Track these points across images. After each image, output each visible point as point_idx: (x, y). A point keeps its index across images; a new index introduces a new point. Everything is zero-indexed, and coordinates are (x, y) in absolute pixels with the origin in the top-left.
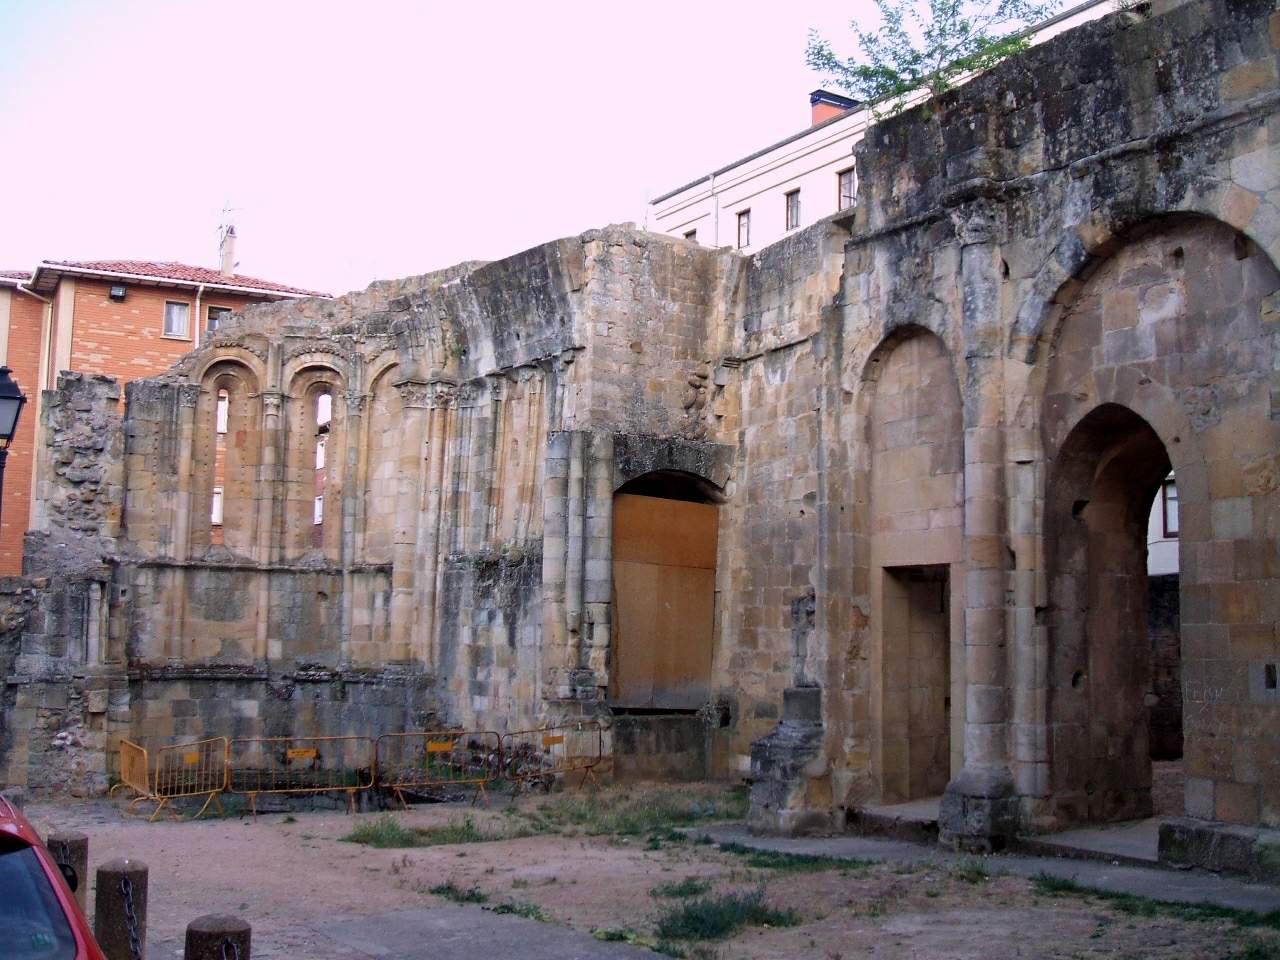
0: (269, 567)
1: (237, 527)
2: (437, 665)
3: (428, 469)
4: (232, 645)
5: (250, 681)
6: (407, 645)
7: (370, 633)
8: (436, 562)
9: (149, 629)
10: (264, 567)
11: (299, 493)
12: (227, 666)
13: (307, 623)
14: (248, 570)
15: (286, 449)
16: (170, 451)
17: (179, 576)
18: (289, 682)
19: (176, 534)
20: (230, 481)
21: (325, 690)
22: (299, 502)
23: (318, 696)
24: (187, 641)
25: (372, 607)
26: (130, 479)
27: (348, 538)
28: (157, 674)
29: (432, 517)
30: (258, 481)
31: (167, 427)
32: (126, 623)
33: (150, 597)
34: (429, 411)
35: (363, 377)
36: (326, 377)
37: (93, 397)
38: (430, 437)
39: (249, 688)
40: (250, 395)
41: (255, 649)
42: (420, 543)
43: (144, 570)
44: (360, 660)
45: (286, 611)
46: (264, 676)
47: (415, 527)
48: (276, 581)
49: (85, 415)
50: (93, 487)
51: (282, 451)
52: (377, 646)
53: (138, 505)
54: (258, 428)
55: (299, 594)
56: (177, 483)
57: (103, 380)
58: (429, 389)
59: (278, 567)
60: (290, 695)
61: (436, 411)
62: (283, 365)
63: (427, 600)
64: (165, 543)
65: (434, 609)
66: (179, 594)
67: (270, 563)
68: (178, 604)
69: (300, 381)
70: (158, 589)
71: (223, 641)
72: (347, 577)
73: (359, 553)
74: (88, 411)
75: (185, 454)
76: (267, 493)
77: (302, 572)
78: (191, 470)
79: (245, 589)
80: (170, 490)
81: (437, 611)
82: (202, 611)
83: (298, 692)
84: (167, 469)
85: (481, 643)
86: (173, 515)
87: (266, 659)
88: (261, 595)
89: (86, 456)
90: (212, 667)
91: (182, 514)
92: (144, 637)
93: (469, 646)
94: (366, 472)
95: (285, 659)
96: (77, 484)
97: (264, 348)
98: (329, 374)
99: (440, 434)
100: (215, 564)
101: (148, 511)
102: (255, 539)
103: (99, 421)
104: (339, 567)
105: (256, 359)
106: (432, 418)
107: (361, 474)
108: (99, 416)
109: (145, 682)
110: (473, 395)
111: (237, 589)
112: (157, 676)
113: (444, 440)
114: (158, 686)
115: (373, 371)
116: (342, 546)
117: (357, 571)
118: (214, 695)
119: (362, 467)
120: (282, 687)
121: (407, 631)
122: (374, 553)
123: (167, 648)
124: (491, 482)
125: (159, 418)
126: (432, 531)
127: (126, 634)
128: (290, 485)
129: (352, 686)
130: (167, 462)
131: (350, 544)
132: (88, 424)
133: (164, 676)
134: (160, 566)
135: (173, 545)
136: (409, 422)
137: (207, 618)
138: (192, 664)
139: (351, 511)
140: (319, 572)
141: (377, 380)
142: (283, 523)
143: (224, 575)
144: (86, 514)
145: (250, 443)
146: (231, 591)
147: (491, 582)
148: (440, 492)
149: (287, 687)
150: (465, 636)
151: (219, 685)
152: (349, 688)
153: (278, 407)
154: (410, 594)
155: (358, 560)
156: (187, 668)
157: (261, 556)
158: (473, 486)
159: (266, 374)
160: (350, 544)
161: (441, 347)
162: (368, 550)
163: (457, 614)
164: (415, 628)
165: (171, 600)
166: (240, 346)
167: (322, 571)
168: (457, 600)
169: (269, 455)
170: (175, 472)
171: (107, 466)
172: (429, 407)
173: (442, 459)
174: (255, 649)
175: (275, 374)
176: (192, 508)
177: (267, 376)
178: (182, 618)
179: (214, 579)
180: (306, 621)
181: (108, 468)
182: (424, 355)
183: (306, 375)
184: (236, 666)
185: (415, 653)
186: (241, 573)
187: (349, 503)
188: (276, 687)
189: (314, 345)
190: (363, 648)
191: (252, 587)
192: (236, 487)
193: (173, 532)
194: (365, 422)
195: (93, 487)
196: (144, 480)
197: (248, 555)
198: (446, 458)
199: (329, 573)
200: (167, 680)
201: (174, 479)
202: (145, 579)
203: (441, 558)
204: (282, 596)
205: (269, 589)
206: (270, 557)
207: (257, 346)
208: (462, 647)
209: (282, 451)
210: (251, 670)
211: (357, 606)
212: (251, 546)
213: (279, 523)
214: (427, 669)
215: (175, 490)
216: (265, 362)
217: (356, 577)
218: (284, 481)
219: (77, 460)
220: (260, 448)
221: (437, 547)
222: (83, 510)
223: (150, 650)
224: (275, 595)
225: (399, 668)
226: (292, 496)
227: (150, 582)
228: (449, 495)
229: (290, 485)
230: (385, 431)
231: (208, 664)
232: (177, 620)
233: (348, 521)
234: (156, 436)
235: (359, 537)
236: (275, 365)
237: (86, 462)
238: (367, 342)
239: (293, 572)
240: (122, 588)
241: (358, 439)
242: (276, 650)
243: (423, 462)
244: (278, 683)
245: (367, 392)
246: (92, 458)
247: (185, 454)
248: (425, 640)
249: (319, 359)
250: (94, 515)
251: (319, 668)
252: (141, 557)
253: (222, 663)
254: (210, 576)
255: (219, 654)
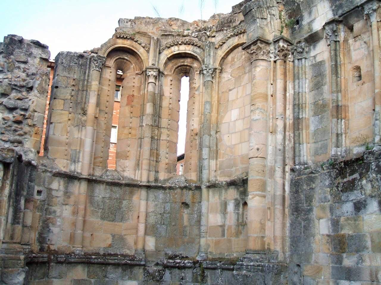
0: (148, 184)
1: (126, 157)
2: (288, 254)
3: (274, 103)
4: (119, 239)
5: (132, 266)
6: (263, 237)
7: (223, 231)
8: (284, 171)
9: (58, 223)
10: (144, 184)
11: (168, 136)
12: (116, 255)
13: (167, 225)
14: (133, 186)
15: (160, 106)
16: (82, 98)
17: (84, 186)
18: (160, 268)
19: (83, 156)
20: (122, 127)
21: (188, 274)
22: (168, 141)
23: (182, 279)
24: (88, 234)
25: (224, 211)
26: (53, 115)
27: (206, 163)
28: (62, 258)
29: (280, 137)
30: (142, 126)
31: (81, 83)
32: (41, 216)
33: (61, 200)
34: (272, 63)
35: (215, 57)
36: (187, 62)
37: (30, 55)
38: (275, 80)
39: (131, 272)
40: (137, 72)
41: (136, 243)
42: (270, 157)
43: (57, 179)
44: (215, 252)
45: (159, 216)
46: (143, 263)
47: (266, 145)
48: (152, 194)
49: (22, 66)
50: (23, 113)
51: (158, 107)
52: (230, 241)
53: (59, 134)
54: (142, 93)
55: (169, 204)
56: (86, 121)
57: (38, 44)
58: (272, 48)
59: (153, 184)
60: (161, 278)
61: (278, 62)
62: (160, 53)
63: (279, 201)
64: (75, 162)
65: (284, 210)
66: (82, 199)
67: (148, 182)
68: (82, 207)
69: (170, 65)
70: (67, 194)
71: (113, 236)
72: (204, 190)
73: (213, 173)
74: (25, 63)
75: (93, 100)
76: (147, 133)
77: (170, 188)
78: (96, 114)
79: (130, 200)
80: (81, 125)
81: (287, 210)
82: (99, 214)
83: (167, 275)
84: (80, 111)
85: (347, 231)
86: (82, 143)
87: (144, 250)
88: (142, 204)
89: (20, 92)
90: (104, 255)
91: (88, 142)
92: (55, 230)
93: (328, 236)
94: (217, 118)
95: (158, 251)
96: (11, 110)
97: (148, 42)
98: (189, 60)
99: (282, 77)
100: (110, 180)
101: (64, 138)
102: (138, 165)
103: (33, 70)
104: (198, 184)
105: (142, 49)
106: (275, 68)
107: (214, 119)
108: (33, 68)
109: (52, 264)
110: (307, 49)
111: (124, 200)
112: (62, 260)
113: (285, 82)
114: (64, 268)
115: (221, 53)
116: (200, 169)
117: (213, 186)
118: (105, 276)
119: (214, 114)
120: (155, 271)
121: (263, 227)
122: (223, 174)
123: (72, 238)
124: (337, 101)
125: (75, 77)
126: (280, 147)
127: (38, 225)
128: (162, 130)
129: (210, 271)
130: (79, 107)
131: (207, 167)
132: (24, 71)
133: (68, 260)
134: (70, 178)
135: (80, 163)
136: (258, 69)
137: (103, 218)
138: (90, 252)
139: (207, 144)
140: (182, 188)
141: (224, 58)
142: (158, 155)
143: (115, 189)
144: (15, 131)
145: (136, 102)
146: (120, 200)
147: (356, 175)
148: (284, 118)
149: (159, 271)
150: (322, 227)
151: (109, 268)
152: (207, 273)
153: (156, 77)
154: (264, 197)
155: (212, 179)
156: (87, 255)
157: (142, 176)
158: (312, 113)
159: (148, 59)
160: (207, 167)
161: (279, 20)
162: (219, 172)
163: (310, 210)
164: (269, 224)
165: (76, 204)
166: (133, 39)
167: (185, 187)
168: (309, 199)
169: (149, 109)
170: (85, 113)
171: (34, 99)
172: (272, 60)
173: (285, 95)
174: (136, 243)
175: (155, 56)
176: (95, 141)
177: (149, 59)
178: (85, 216)
179: (108, 191)
180: (173, 224)
181: (36, 100)
182: (267, 25)
183: (174, 61)
184: (122, 255)
185: (269, 245)
186: (127, 188)
187: (206, 138)
188: (151, 271)
189: (180, 40)
190: (217, 243)
191: (135, 198)
192: (126, 131)
193: (81, 155)
194: (215, 86)
195: (23, 113)
196: (63, 116)
197: (132, 177)
198: (288, 95)
199: (190, 189)
200: (70, 263)
201: (84, 118)
202: (57, 185)
203: (287, 169)
204: (156, 205)
205: (147, 200)
206: (148, 177)
207: (143, 40)
208: (318, 237)
209: (158, 107)
210: (133, 258)
211: (214, 213)
212: (135, 170)
213: (155, 154)
214: (281, 258)
215: (84, 126)
216: (148, 51)
217: (211, 191)
218: (158, 127)
219: (14, 94)
220: (143, 106)
221: (284, 161)
222: (13, 128)
223: (58, 239)
224: (152, 204)
225: (257, 257)
226: (164, 137)
227: (62, 188)
228: (291, 122)
229: (162, 130)
230: (230, 90)
231: (102, 253)
232: (80, 218)
233: (205, 152)
234: (73, 88)
235: (213, 163)
236: (155, 51)
237: (20, 95)
238: (217, 35)
239: (164, 188)
240: (37, 188)
241: (212, 97)
242: (151, 244)
243: (269, 97)
244: (152, 269)
245: (217, 65)
246: (24, 93)
247: (93, 100)
248: (278, 233)
249: (183, 49)
250: (21, 132)
251: (182, 258)
252: (56, 169)
253: (112, 253)
254: (105, 189)
255: (110, 246)
